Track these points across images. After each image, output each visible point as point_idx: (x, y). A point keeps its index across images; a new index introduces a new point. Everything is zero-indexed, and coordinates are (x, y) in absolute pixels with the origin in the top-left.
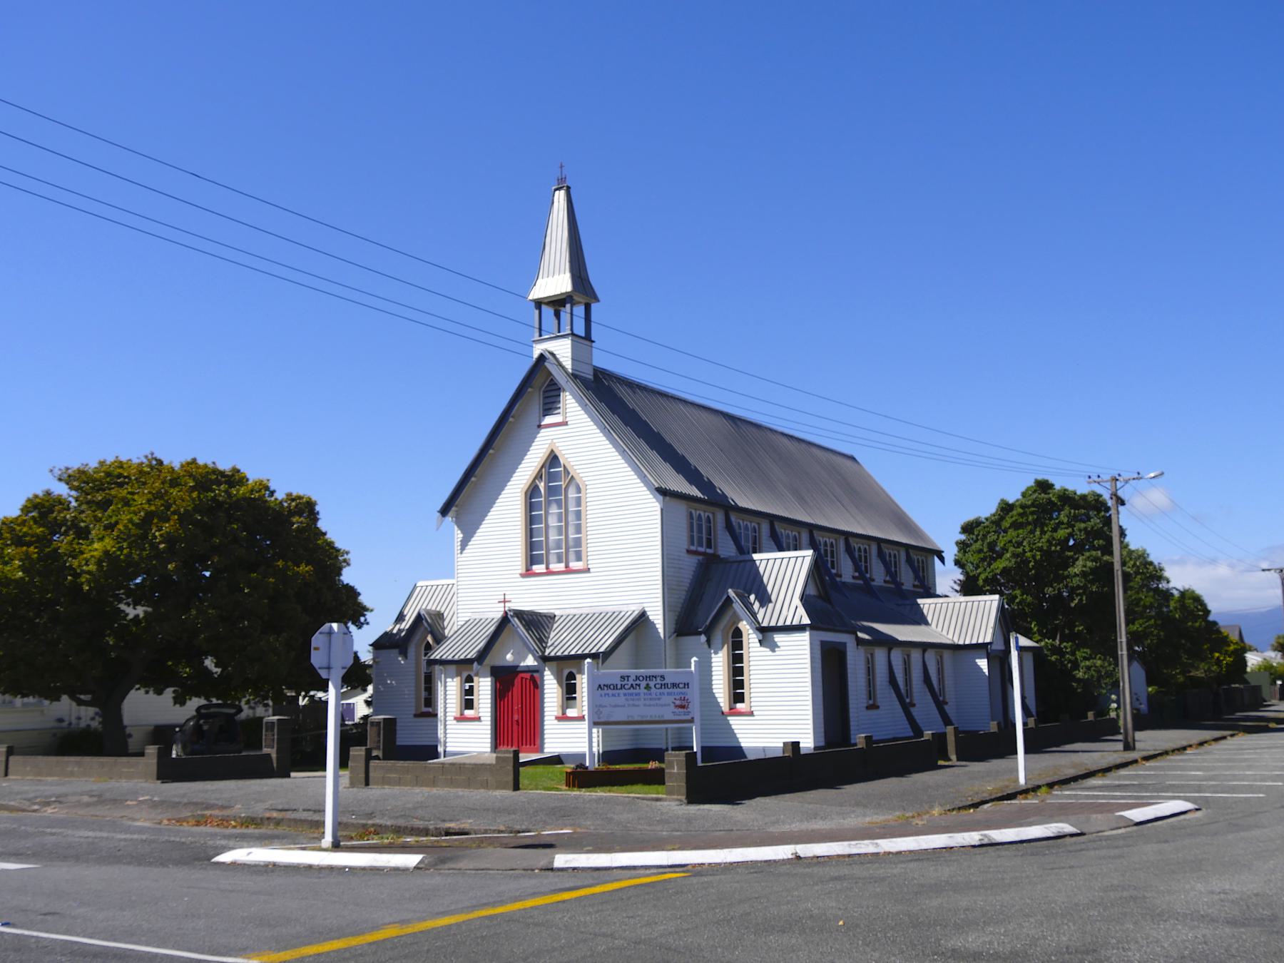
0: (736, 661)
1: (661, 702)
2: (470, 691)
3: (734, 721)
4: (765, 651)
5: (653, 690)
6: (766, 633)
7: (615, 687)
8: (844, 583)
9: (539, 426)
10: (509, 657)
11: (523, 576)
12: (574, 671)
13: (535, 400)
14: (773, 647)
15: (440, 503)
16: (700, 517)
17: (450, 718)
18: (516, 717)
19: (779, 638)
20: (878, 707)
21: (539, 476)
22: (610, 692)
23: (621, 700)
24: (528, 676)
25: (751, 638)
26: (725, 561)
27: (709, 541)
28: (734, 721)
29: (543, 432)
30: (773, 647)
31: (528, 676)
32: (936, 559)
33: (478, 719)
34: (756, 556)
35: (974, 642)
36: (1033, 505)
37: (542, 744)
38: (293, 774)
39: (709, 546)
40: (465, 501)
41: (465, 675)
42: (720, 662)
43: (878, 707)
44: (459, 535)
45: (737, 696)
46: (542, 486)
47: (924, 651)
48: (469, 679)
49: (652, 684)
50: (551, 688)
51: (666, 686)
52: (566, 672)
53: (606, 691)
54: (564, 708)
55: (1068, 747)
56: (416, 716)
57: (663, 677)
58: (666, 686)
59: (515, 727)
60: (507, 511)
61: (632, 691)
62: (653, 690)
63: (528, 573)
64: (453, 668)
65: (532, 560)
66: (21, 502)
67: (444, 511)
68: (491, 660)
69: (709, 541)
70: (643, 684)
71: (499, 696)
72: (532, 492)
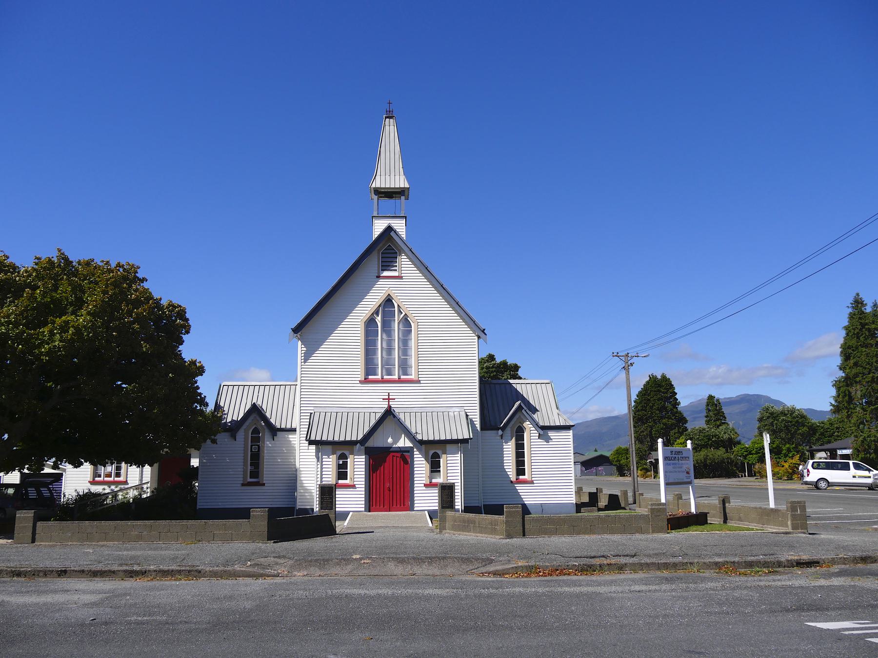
0: (520, 447)
2: (344, 466)
3: (519, 487)
4: (542, 442)
6: (545, 430)
9: (378, 277)
10: (390, 440)
11: (361, 382)
12: (439, 452)
13: (374, 261)
14: (548, 439)
15: (294, 325)
18: (388, 485)
19: (551, 434)
21: (377, 312)
24: (399, 455)
25: (530, 434)
28: (519, 487)
29: (381, 282)
30: (548, 439)
31: (399, 455)
33: (353, 486)
35: (342, 439)
36: (493, 367)
37: (413, 504)
40: (312, 326)
41: (339, 453)
42: (509, 449)
44: (300, 348)
45: (520, 471)
46: (379, 319)
48: (343, 457)
50: (420, 465)
52: (431, 452)
54: (431, 478)
56: (243, 485)
59: (387, 492)
60: (348, 335)
63: (366, 381)
64: (330, 447)
65: (370, 369)
66: (86, 257)
67: (297, 330)
68: (370, 444)
71: (372, 470)
72: (370, 322)
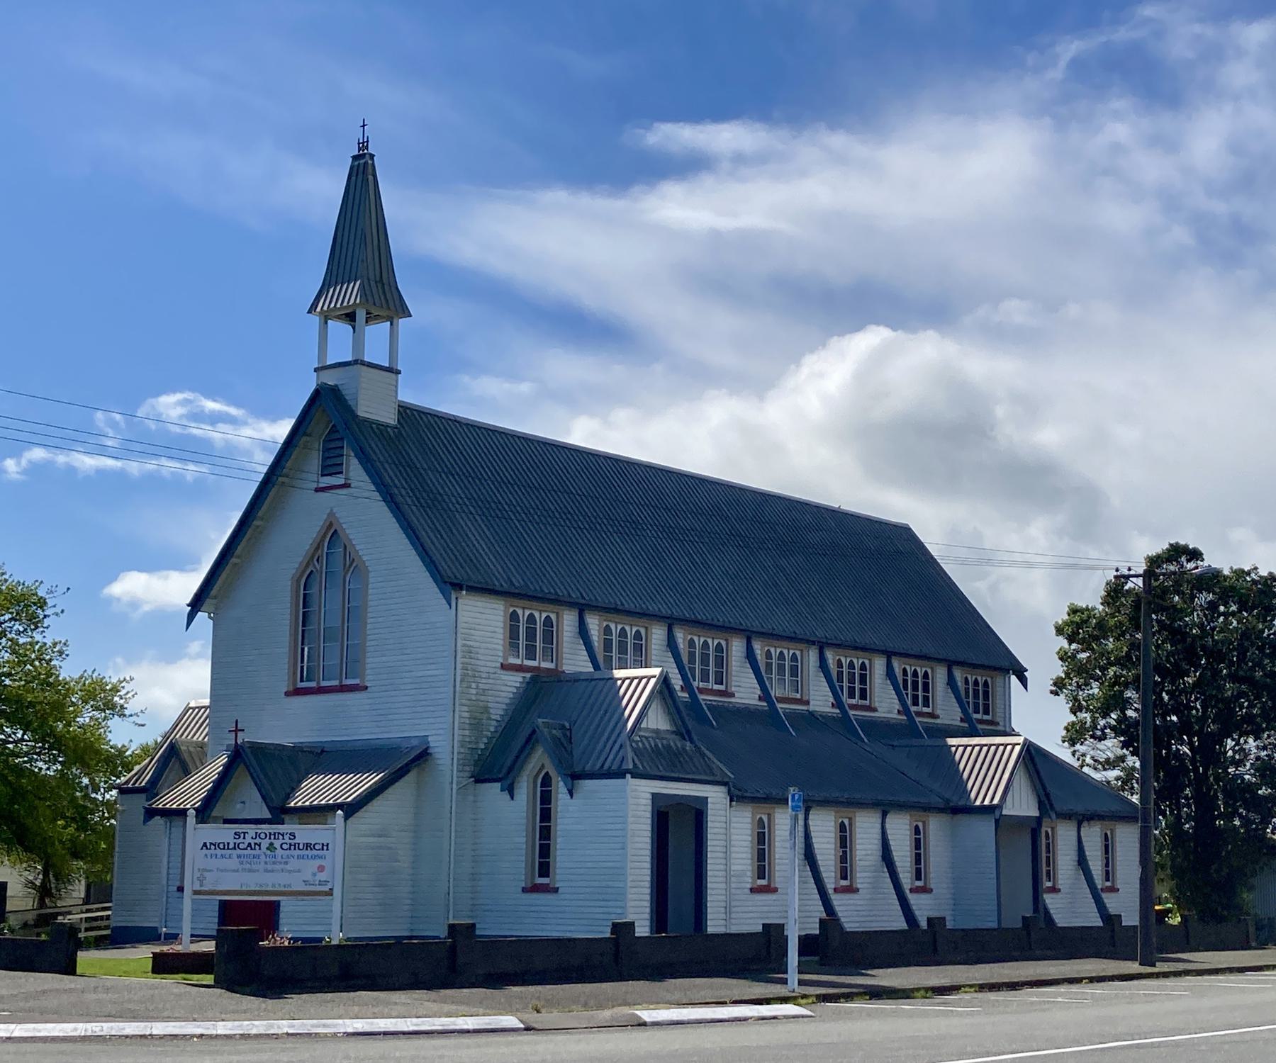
1: (288, 867)
5: (279, 852)
7: (226, 846)
8: (811, 714)
16: (976, 683)
17: (831, 891)
20: (775, 890)
22: (219, 852)
23: (233, 863)
26: (576, 679)
27: (926, 699)
32: (1013, 678)
34: (618, 673)
38: (760, 929)
39: (863, 696)
43: (775, 890)
47: (884, 815)
49: (277, 844)
51: (296, 846)
53: (213, 851)
55: (869, 972)
57: (293, 835)
58: (296, 846)
61: (249, 851)
62: (279, 852)
69: (926, 699)
70: (265, 843)
